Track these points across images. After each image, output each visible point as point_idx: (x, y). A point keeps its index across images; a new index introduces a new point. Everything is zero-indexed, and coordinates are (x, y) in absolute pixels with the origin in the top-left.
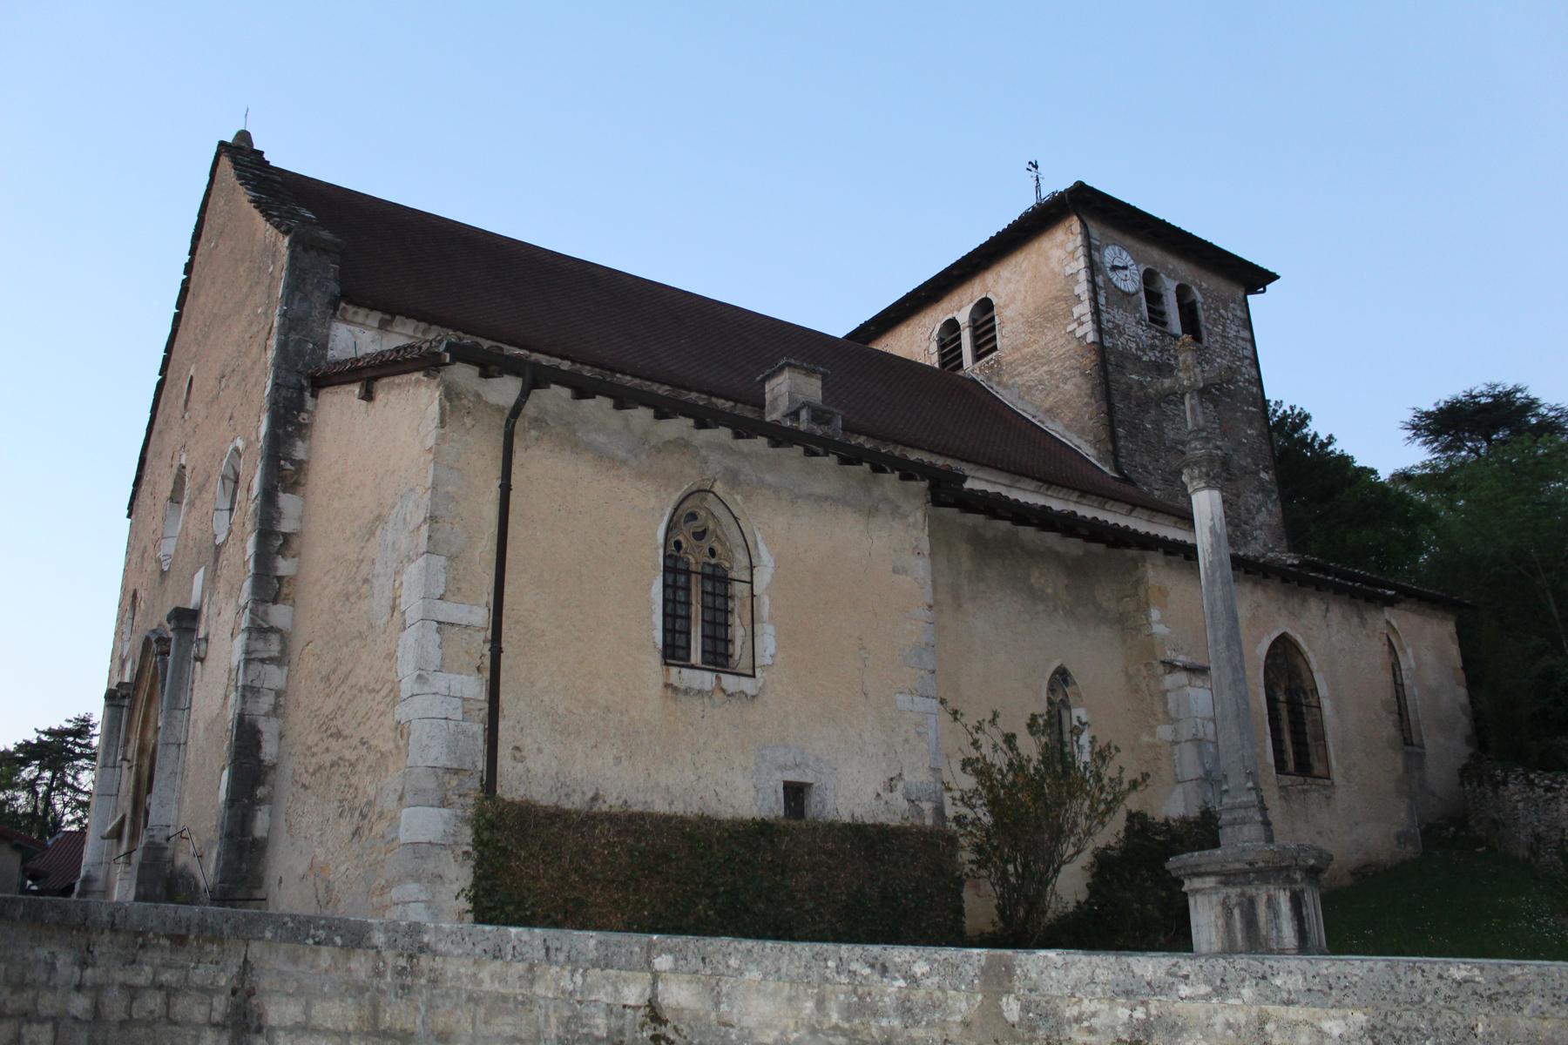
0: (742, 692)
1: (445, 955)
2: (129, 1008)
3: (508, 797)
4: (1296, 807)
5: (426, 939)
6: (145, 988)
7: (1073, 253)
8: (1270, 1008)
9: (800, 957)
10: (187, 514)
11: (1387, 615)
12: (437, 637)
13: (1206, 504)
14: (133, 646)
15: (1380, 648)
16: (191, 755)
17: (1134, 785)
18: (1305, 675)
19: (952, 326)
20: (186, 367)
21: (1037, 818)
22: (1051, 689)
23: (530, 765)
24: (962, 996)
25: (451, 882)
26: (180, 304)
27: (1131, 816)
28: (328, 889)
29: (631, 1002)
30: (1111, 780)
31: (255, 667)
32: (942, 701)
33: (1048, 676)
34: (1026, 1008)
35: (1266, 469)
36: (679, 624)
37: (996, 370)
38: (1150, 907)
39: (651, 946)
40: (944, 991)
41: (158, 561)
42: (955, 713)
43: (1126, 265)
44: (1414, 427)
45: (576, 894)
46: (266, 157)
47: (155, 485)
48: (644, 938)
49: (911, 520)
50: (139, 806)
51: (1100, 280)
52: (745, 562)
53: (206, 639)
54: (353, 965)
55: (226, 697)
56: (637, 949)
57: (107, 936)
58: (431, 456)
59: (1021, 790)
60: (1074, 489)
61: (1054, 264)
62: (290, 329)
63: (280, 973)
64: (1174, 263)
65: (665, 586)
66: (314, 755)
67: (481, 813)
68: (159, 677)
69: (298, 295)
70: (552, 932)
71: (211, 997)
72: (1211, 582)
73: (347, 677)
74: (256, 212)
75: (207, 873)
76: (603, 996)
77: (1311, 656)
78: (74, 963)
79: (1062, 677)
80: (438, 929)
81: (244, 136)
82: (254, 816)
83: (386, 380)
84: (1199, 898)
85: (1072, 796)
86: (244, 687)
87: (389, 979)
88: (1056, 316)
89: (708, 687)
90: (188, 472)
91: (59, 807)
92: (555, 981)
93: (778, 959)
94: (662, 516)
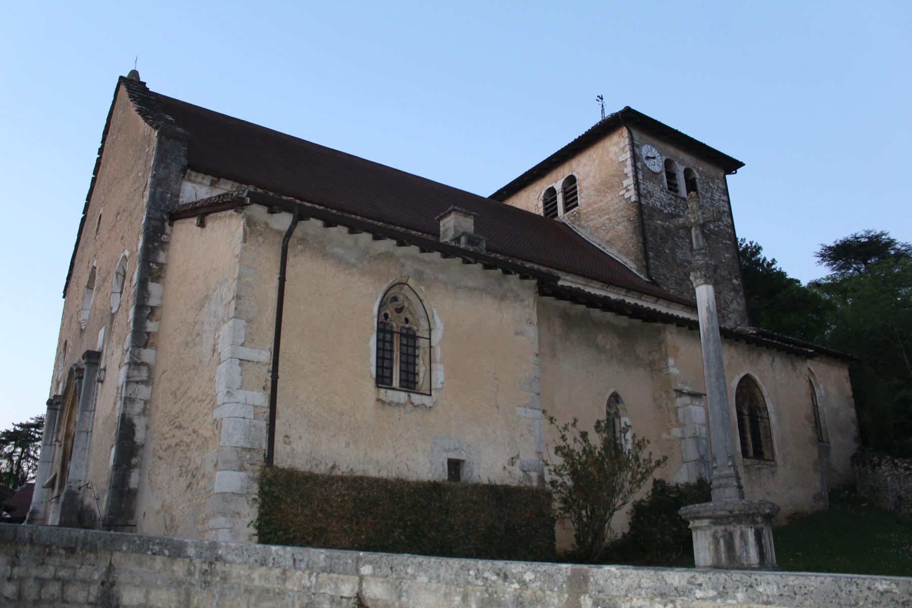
0: (424, 405)
1: (231, 563)
2: (39, 592)
3: (280, 466)
4: (754, 478)
5: (220, 552)
7: (624, 148)
9: (452, 568)
10: (96, 295)
11: (808, 365)
12: (239, 369)
13: (704, 294)
14: (63, 374)
16: (94, 438)
17: (658, 463)
18: (760, 399)
19: (551, 192)
20: (97, 209)
21: (599, 482)
22: (609, 406)
24: (555, 595)
25: (245, 517)
26: (96, 172)
27: (656, 482)
28: (172, 520)
29: (346, 595)
30: (644, 460)
31: (133, 386)
32: (544, 412)
33: (607, 397)
35: (736, 278)
36: (386, 363)
37: (577, 217)
39: (358, 559)
40: (543, 591)
41: (79, 323)
42: (551, 419)
43: (654, 156)
44: (822, 255)
46: (147, 86)
47: (79, 279)
48: (355, 554)
49: (526, 303)
50: (64, 468)
51: (639, 165)
52: (427, 326)
53: (105, 370)
54: (176, 568)
55: (115, 404)
56: (350, 561)
58: (238, 260)
59: (590, 466)
60: (623, 287)
61: (612, 155)
63: (131, 572)
64: (682, 155)
65: (378, 340)
67: (263, 475)
68: (76, 393)
69: (163, 165)
70: (297, 550)
71: (89, 586)
72: (707, 340)
73: (186, 392)
74: (139, 117)
75: (101, 509)
76: (328, 590)
77: (763, 388)
78: (7, 564)
79: (615, 398)
81: (134, 73)
82: (129, 476)
83: (212, 215)
84: (699, 532)
85: (621, 469)
86: (126, 398)
87: (197, 577)
88: (613, 186)
89: (403, 401)
90: (97, 271)
91: (25, 469)
92: (300, 579)
93: (438, 569)
94: (377, 298)
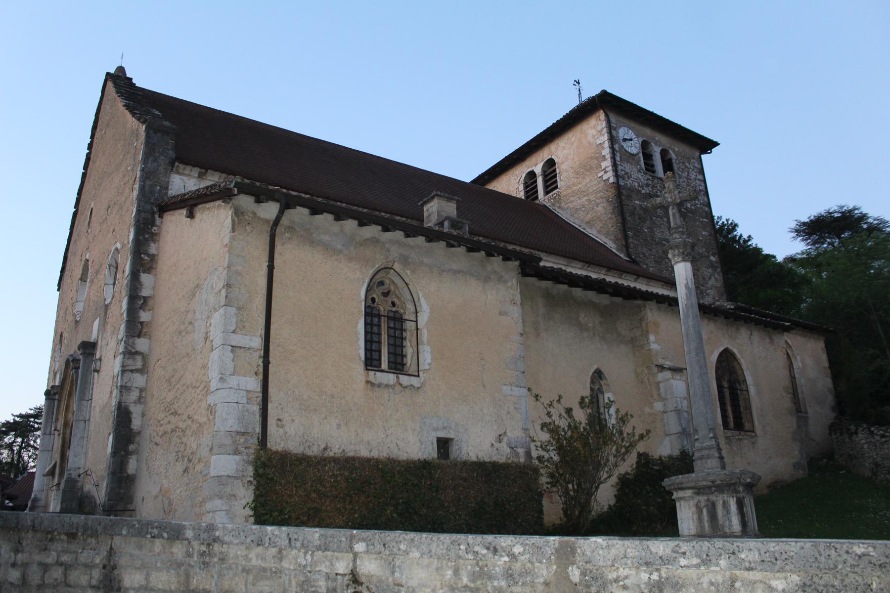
1: (228, 544)
3: (274, 448)
5: (217, 534)
6: (51, 565)
8: (738, 572)
9: (443, 543)
10: (89, 288)
12: (231, 355)
13: (682, 271)
14: (60, 365)
15: (781, 357)
16: (92, 427)
17: (642, 437)
18: (739, 372)
19: (532, 175)
20: (88, 203)
21: (585, 456)
22: (592, 382)
23: (287, 429)
24: (544, 566)
25: (241, 499)
26: (86, 167)
27: (640, 455)
28: (170, 504)
29: (341, 571)
30: (628, 434)
31: (128, 375)
32: (529, 390)
34: (583, 574)
35: (713, 255)
37: (558, 199)
38: (652, 508)
39: (352, 537)
40: (532, 563)
41: (74, 315)
42: (536, 396)
43: (631, 138)
44: (797, 231)
45: (315, 505)
46: (134, 81)
47: (73, 272)
48: (348, 532)
49: (509, 284)
50: (63, 457)
51: (616, 147)
52: (413, 309)
53: (100, 359)
54: (174, 550)
55: (111, 392)
56: (344, 539)
57: (30, 534)
58: (227, 249)
59: (575, 441)
60: (604, 267)
61: (590, 138)
62: (146, 178)
63: (131, 555)
64: (659, 137)
66: (161, 425)
67: (258, 458)
69: (151, 159)
70: (292, 529)
72: (687, 316)
73: (180, 380)
74: (127, 112)
75: (101, 495)
76: (324, 568)
77: (742, 361)
79: (598, 375)
80: (224, 528)
81: (121, 69)
82: (127, 462)
83: (200, 206)
84: (682, 502)
85: (605, 443)
86: (121, 386)
87: (195, 558)
88: (591, 168)
89: (391, 383)
90: (90, 264)
91: (26, 458)
92: (295, 558)
93: (430, 545)
94: (363, 283)
